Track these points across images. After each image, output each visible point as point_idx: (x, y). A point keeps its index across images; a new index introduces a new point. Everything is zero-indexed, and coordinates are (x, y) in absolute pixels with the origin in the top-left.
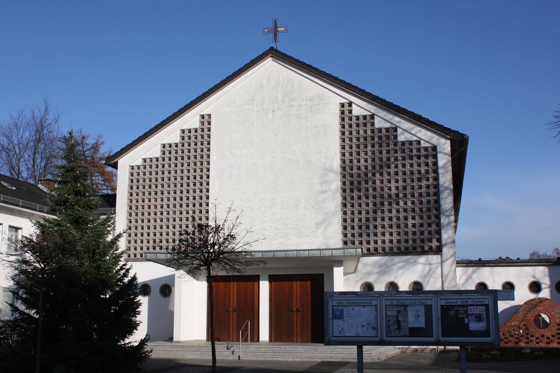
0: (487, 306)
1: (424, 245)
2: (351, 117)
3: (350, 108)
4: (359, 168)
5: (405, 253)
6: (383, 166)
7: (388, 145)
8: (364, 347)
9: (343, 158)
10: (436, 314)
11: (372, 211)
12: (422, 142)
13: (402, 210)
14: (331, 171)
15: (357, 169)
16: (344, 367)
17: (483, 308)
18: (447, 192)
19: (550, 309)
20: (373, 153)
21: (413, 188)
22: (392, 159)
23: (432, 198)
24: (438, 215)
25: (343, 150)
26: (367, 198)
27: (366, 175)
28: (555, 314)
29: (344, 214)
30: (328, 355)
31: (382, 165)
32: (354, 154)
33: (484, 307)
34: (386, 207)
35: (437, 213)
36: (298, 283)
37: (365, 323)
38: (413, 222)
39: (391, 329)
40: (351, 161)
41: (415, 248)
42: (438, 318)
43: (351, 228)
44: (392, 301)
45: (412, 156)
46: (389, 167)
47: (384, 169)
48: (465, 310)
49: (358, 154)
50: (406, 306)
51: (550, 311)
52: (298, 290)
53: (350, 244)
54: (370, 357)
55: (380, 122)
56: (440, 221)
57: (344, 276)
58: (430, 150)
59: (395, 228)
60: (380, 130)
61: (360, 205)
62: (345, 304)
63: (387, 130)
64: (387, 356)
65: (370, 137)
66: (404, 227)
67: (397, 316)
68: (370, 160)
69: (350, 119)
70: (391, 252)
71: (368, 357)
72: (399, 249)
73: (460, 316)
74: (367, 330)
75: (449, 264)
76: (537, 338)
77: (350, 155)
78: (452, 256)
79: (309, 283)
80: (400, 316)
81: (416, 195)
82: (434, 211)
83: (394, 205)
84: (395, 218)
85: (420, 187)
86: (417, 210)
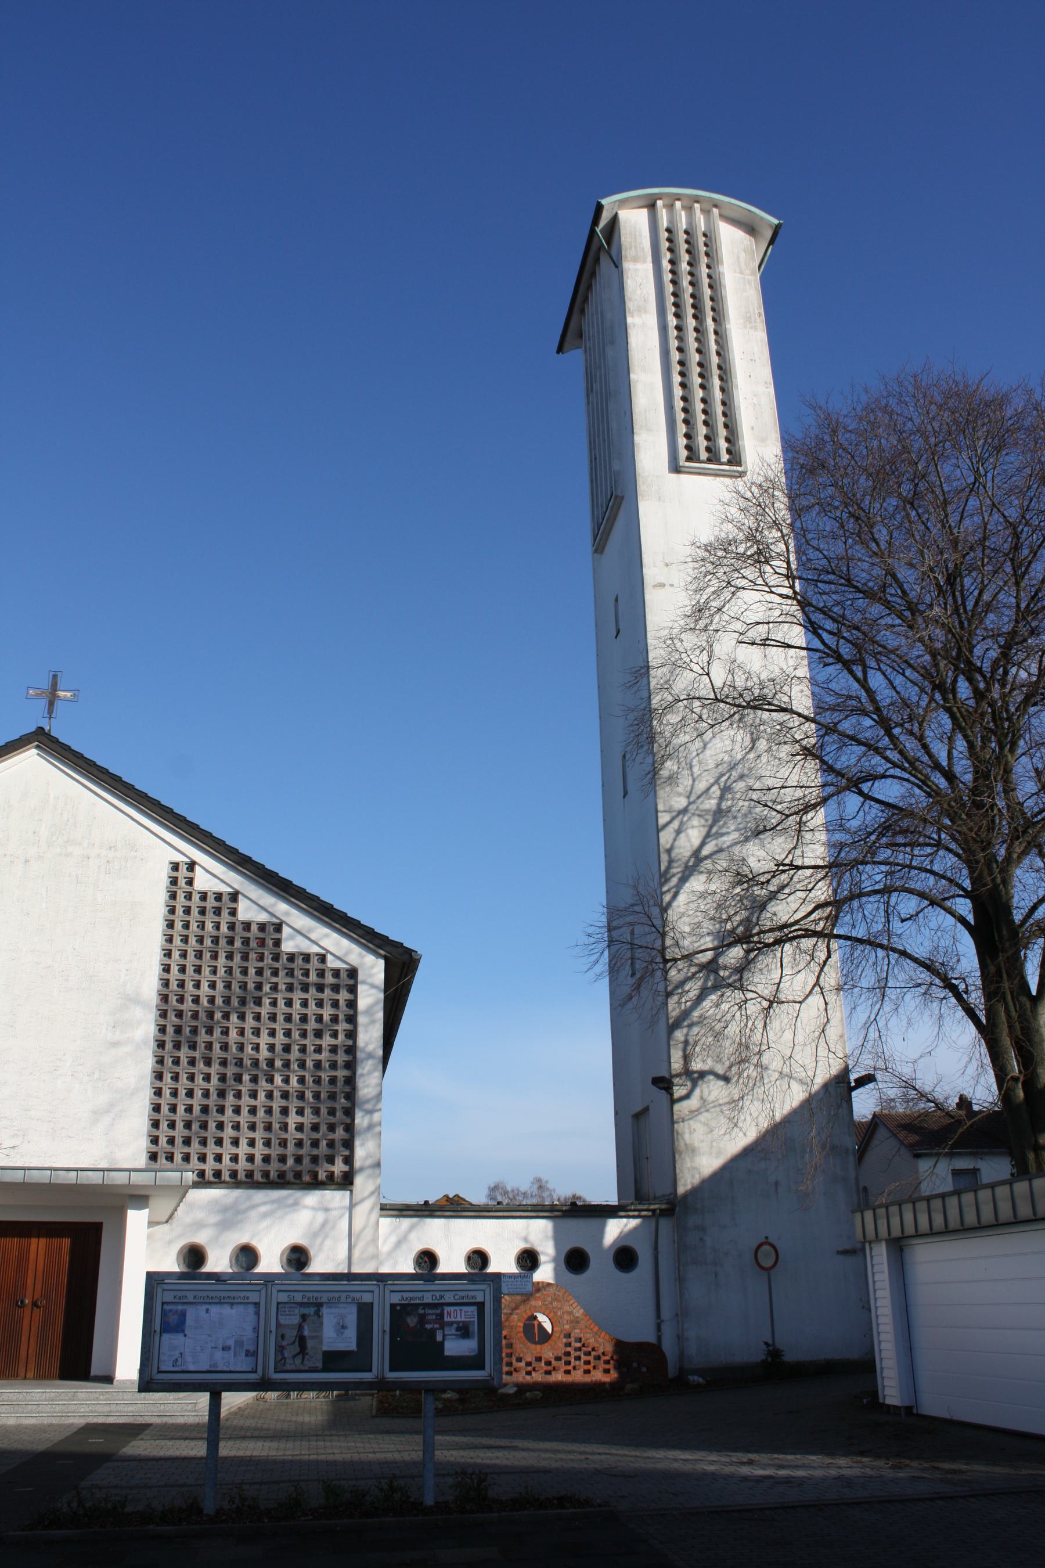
0: (481, 1306)
1: (317, 1169)
2: (191, 893)
3: (190, 875)
4: (196, 1000)
5: (277, 1183)
6: (248, 1000)
7: (261, 958)
8: (224, 1395)
9: (166, 976)
10: (381, 1322)
11: (217, 1092)
12: (329, 957)
13: (279, 1094)
14: (135, 1000)
15: (193, 1001)
16: (140, 1437)
17: (474, 1309)
18: (370, 1062)
19: (555, 1304)
20: (229, 971)
21: (303, 1049)
22: (267, 988)
23: (341, 1073)
24: (351, 1108)
25: (166, 959)
26: (208, 1062)
27: (210, 1015)
28: (563, 1313)
29: (155, 1093)
30: (99, 1408)
31: (245, 998)
32: (190, 970)
33: (475, 1308)
34: (246, 1086)
35: (349, 1105)
36: (43, 1241)
37: (231, 1342)
38: (300, 1119)
39: (286, 1355)
40: (182, 984)
41: (298, 1175)
42: (384, 1331)
43: (168, 1125)
44: (292, 1294)
45: (308, 984)
46: (258, 1002)
47: (247, 1006)
48: (437, 1315)
49: (198, 970)
50: (319, 1305)
51: (553, 1308)
52: (42, 1263)
53: (162, 1160)
54: (195, 1411)
55: (247, 909)
56: (353, 1120)
57: (149, 1227)
58: (343, 975)
59: (262, 1130)
60: (247, 926)
61: (191, 1078)
62: (191, 1300)
63: (262, 927)
64: (229, 1409)
65: (226, 937)
66: (280, 1128)
67: (300, 1327)
68: (220, 985)
69: (189, 896)
70: (250, 1182)
71: (189, 1411)
72: (266, 1174)
73: (428, 1326)
74: (235, 1356)
75: (365, 1211)
76: (529, 1364)
77: (179, 971)
78: (372, 1193)
79: (66, 1242)
80: (306, 1327)
81: (309, 1064)
82: (343, 1100)
83: (263, 1083)
84: (263, 1110)
85: (319, 1050)
86: (309, 1095)
